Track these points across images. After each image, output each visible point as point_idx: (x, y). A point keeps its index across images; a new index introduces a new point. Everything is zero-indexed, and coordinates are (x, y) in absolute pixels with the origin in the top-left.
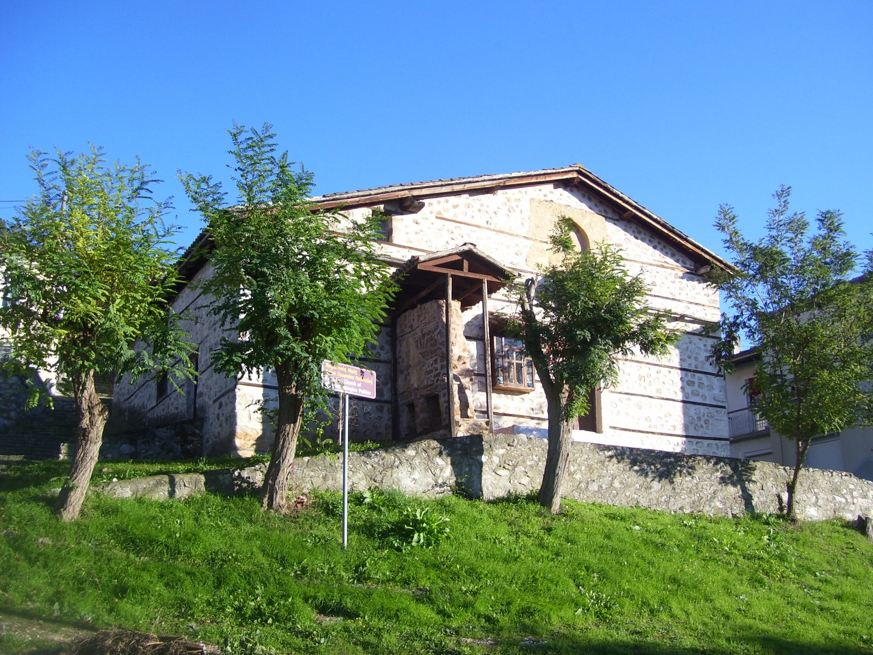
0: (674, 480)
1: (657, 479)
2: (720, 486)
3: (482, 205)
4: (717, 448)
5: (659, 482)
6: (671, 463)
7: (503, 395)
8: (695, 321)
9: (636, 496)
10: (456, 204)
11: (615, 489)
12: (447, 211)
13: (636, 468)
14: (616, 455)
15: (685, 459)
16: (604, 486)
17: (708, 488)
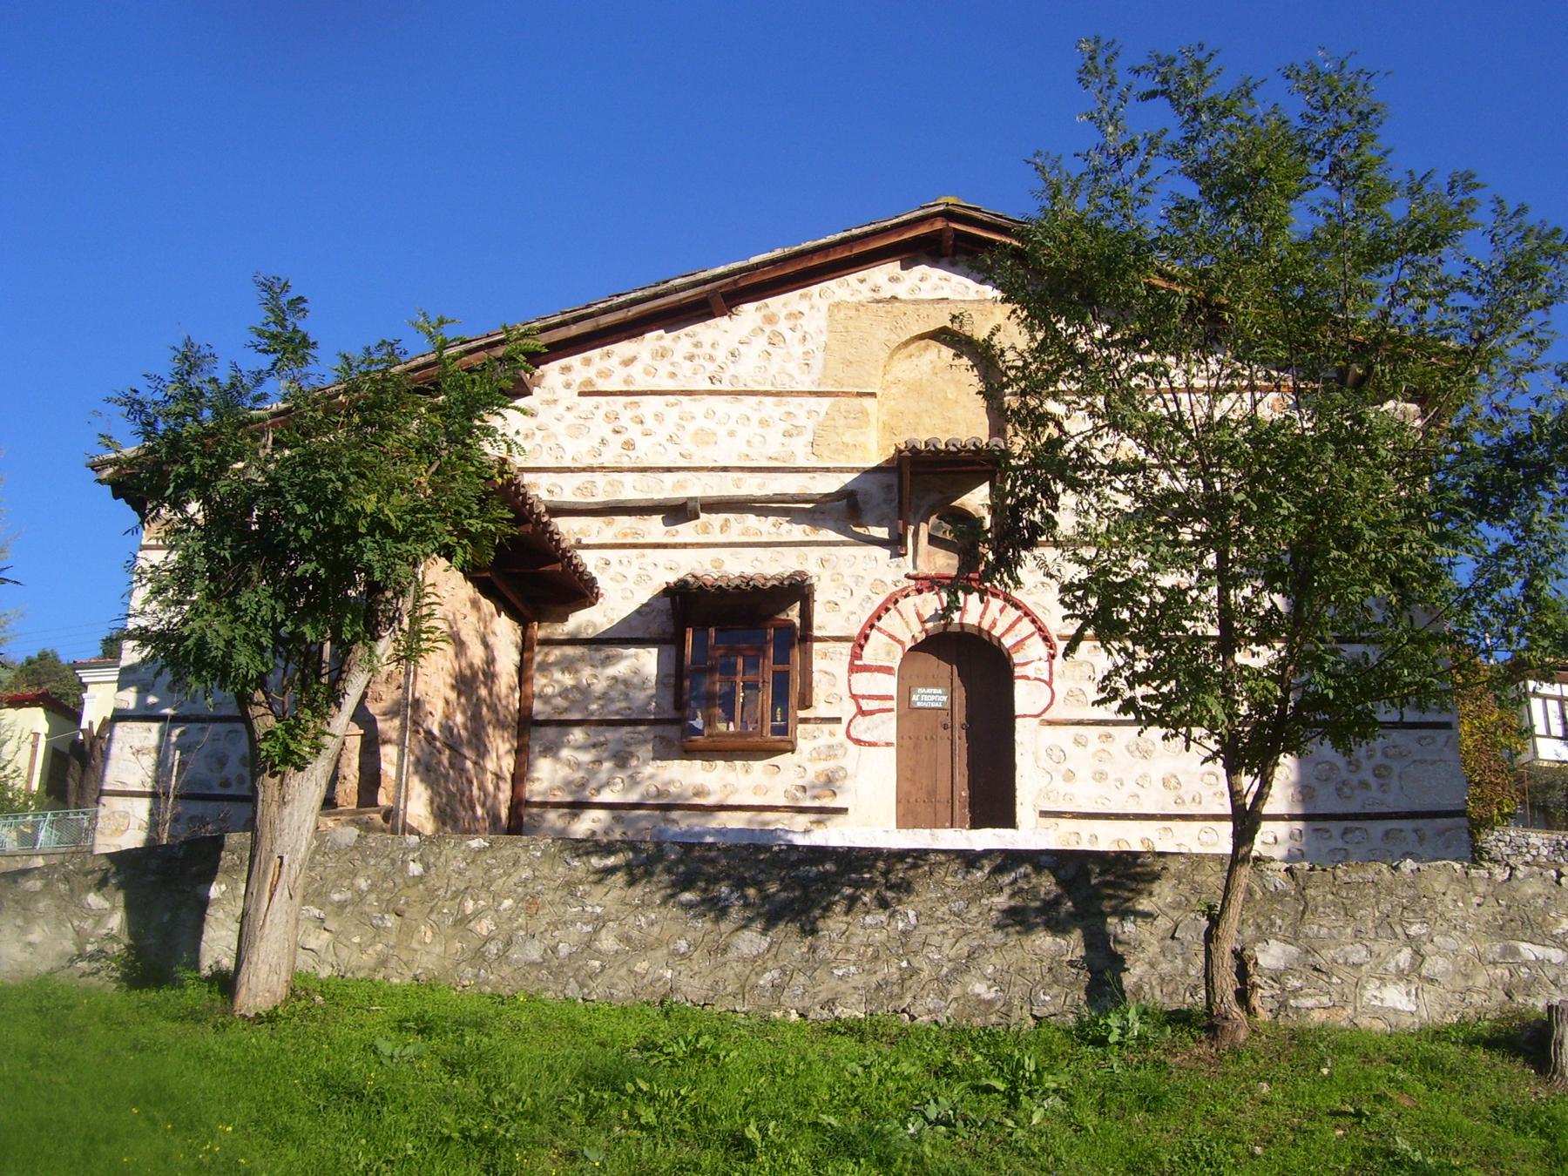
0: (820, 924)
1: (758, 925)
2: (998, 937)
3: (697, 345)
4: (1421, 840)
5: (764, 932)
6: (824, 877)
7: (720, 764)
8: (852, 470)
9: (669, 974)
10: (631, 354)
11: (599, 954)
12: (602, 374)
13: (687, 896)
14: (629, 867)
15: (881, 865)
16: (564, 949)
17: (947, 943)
